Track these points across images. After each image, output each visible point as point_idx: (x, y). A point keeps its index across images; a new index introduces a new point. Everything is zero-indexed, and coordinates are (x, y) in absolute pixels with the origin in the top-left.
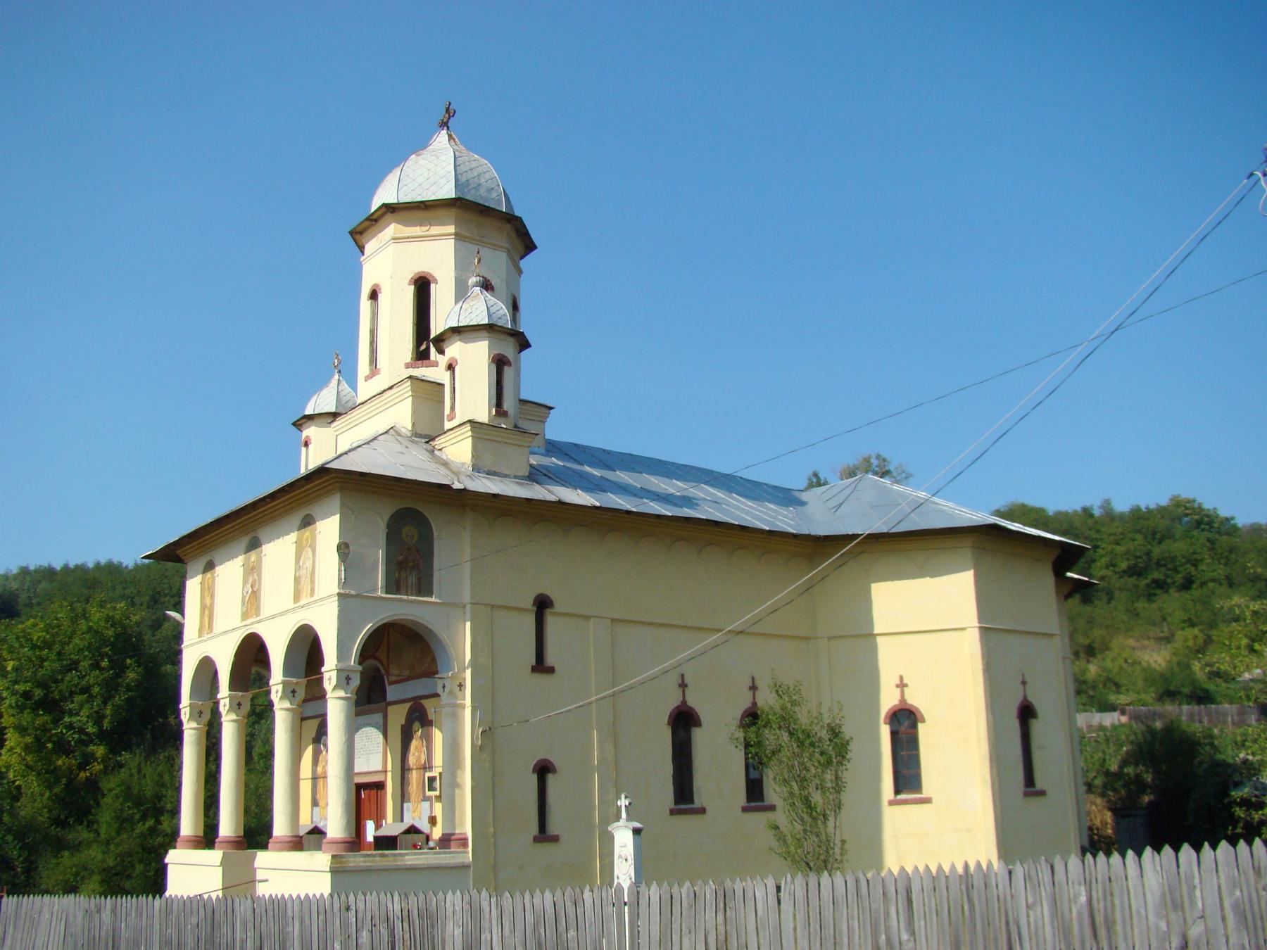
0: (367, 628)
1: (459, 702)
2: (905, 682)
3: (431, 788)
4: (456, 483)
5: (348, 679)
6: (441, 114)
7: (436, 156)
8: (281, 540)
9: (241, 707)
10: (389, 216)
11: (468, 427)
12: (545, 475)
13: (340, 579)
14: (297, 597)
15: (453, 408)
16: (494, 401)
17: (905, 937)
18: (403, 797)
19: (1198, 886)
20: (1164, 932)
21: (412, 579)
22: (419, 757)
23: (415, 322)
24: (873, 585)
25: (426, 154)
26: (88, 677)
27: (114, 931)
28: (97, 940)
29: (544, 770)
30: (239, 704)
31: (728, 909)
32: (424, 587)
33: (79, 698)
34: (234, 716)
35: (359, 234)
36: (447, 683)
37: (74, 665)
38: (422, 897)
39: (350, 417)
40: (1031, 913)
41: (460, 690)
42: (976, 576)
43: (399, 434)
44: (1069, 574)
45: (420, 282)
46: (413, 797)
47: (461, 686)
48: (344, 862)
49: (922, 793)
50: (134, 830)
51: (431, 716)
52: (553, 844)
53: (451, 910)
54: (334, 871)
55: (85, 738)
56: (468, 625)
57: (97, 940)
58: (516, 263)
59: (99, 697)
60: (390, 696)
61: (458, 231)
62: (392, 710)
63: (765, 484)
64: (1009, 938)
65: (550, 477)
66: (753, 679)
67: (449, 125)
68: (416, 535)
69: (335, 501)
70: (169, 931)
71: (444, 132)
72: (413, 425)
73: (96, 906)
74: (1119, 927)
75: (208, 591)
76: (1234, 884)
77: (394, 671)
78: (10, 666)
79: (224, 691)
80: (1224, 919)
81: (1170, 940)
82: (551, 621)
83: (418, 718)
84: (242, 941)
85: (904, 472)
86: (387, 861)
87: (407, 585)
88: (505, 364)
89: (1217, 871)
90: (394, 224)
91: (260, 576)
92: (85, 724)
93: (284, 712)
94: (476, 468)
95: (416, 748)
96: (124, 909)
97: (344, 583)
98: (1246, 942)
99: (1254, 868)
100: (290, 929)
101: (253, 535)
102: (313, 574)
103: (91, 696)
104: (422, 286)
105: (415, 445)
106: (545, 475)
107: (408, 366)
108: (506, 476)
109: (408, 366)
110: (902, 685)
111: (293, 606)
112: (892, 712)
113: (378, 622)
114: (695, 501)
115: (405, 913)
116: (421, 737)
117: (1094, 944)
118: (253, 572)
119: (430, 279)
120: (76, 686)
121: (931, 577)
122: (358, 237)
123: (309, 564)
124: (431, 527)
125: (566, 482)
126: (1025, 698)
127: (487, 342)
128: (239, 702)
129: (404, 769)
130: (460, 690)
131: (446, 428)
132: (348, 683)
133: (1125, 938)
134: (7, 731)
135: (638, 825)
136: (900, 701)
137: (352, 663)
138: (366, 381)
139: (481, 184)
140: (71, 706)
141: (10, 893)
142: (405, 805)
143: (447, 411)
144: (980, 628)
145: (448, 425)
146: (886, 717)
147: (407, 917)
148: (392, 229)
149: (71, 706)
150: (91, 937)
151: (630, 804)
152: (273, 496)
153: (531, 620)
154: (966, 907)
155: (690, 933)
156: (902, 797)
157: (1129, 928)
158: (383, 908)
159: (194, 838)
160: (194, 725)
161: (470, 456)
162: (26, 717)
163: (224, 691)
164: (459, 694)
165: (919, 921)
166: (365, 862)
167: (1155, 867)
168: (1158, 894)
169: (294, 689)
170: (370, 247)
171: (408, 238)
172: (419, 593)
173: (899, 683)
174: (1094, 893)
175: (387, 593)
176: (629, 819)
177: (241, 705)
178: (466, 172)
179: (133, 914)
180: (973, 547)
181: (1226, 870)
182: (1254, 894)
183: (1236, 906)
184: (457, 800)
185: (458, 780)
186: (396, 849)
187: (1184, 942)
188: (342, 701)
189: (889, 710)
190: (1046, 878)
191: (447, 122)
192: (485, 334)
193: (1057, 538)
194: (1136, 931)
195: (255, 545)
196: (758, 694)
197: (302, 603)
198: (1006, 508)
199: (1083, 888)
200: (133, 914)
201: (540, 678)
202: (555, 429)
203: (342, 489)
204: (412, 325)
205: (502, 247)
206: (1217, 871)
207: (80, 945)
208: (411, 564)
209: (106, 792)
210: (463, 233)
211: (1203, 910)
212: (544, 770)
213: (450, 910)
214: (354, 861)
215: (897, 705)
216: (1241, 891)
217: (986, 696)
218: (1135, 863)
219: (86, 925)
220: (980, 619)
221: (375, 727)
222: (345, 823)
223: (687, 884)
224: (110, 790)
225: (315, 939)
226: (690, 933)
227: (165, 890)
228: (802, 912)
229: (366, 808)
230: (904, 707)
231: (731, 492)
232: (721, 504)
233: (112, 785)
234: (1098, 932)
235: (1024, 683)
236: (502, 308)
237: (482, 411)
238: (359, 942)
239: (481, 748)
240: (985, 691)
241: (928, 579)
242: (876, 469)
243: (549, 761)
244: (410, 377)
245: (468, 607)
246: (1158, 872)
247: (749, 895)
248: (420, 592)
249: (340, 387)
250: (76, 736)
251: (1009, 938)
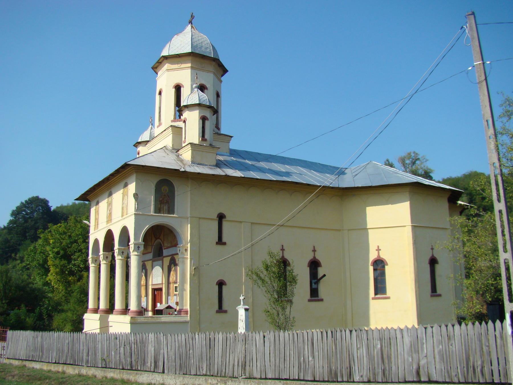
0: (147, 227)
1: (185, 256)
2: (380, 248)
3: (176, 291)
4: (182, 168)
5: (139, 247)
6: (189, 18)
7: (184, 35)
8: (118, 192)
10: (165, 61)
11: (189, 146)
12: (225, 164)
13: (135, 208)
14: (122, 216)
15: (185, 138)
16: (201, 135)
17: (310, 359)
18: (168, 294)
19: (425, 343)
20: (411, 362)
21: (166, 208)
22: (173, 278)
23: (176, 103)
24: (367, 208)
25: (181, 35)
26: (81, 246)
27: (42, 345)
28: (37, 348)
29: (221, 284)
30: (107, 257)
31: (246, 344)
32: (171, 211)
33: (77, 254)
34: (105, 262)
35: (155, 68)
36: (181, 249)
37: (76, 241)
38: (141, 335)
39: (152, 142)
40: (358, 351)
41: (186, 252)
42: (411, 204)
43: (167, 149)
44: (459, 202)
45: (177, 87)
46: (171, 294)
47: (186, 250)
49: (386, 295)
50: (84, 305)
51: (177, 262)
52: (225, 313)
53: (150, 340)
54: (131, 323)
55: (80, 269)
56: (189, 225)
57: (37, 348)
58: (219, 79)
59: (85, 253)
60: (164, 254)
61: (192, 66)
62: (165, 259)
63: (330, 166)
64: (350, 362)
65: (226, 165)
66: (314, 247)
67: (192, 22)
68: (168, 190)
69: (134, 177)
70: (59, 345)
71: (190, 25)
72: (173, 145)
73: (36, 335)
74: (393, 359)
75: (97, 212)
76: (440, 342)
77: (166, 244)
78: (51, 241)
79: (101, 252)
80: (434, 358)
81: (412, 365)
82: (225, 224)
83: (173, 263)
84: (82, 350)
85: (425, 159)
87: (163, 210)
88: (206, 120)
89: (433, 337)
90: (167, 64)
91: (112, 207)
92: (80, 264)
93: (119, 260)
94: (193, 162)
95: (172, 274)
96: (45, 337)
97: (137, 210)
98: (443, 368)
99: (448, 336)
100: (98, 346)
101: (109, 191)
102: (127, 206)
103: (82, 253)
104: (178, 88)
105: (173, 154)
106: (225, 164)
107: (172, 121)
108: (206, 165)
109: (172, 121)
110: (378, 250)
111: (121, 218)
112: (374, 261)
113: (151, 225)
114: (291, 174)
115: (135, 341)
116: (174, 271)
117: (382, 365)
118: (110, 204)
119: (181, 86)
120: (76, 249)
121: (392, 204)
122: (155, 69)
123: (126, 202)
124: (174, 186)
125: (233, 167)
126: (433, 255)
127: (198, 111)
129: (168, 283)
130: (186, 252)
131: (183, 146)
132: (138, 249)
133: (395, 364)
134: (50, 267)
135: (247, 307)
136: (377, 256)
137: (140, 241)
138: (157, 128)
139: (202, 46)
140: (75, 257)
141: (10, 329)
142: (169, 297)
143: (183, 139)
144: (412, 226)
145: (184, 145)
146: (372, 263)
147: (136, 343)
148: (167, 66)
149: (75, 257)
150: (35, 347)
151: (244, 298)
152: (112, 175)
153: (216, 224)
154: (334, 348)
155: (233, 353)
156: (376, 296)
157: (396, 360)
158: (128, 339)
159: (93, 309)
160: (93, 265)
161: (191, 157)
162: (57, 262)
163: (101, 252)
164: (186, 253)
165: (316, 352)
166: (144, 320)
167: (408, 334)
168: (409, 345)
170: (159, 73)
171: (172, 69)
172: (169, 213)
173: (377, 249)
174: (383, 344)
175: (155, 213)
176: (244, 304)
178: (196, 41)
179: (48, 339)
180: (409, 192)
181: (436, 336)
182: (447, 347)
183: (439, 352)
184: (184, 295)
185: (185, 288)
186: (162, 315)
187: (418, 367)
188: (136, 256)
189: (373, 260)
190: (365, 337)
191: (191, 21)
192: (197, 107)
193: (448, 187)
194: (399, 361)
195: (110, 194)
196: (316, 253)
197: (124, 217)
198: (468, 173)
199: (379, 342)
200: (48, 339)
201: (220, 247)
202: (234, 145)
203: (136, 172)
204: (174, 105)
205: (211, 71)
206: (433, 337)
207: (31, 350)
208: (165, 202)
209: (74, 291)
210: (194, 66)
211: (426, 354)
212: (221, 284)
213: (150, 340)
214: (140, 319)
215: (376, 258)
216: (442, 346)
217: (414, 255)
218: (400, 332)
219: (33, 342)
220: (412, 222)
221: (160, 266)
222: (137, 305)
223: (233, 333)
224: (75, 290)
225: (106, 350)
226: (233, 353)
227: (83, 329)
228: (272, 346)
229: (158, 298)
230: (379, 259)
231: (311, 170)
232: (302, 175)
233: (76, 288)
234: (384, 361)
235: (432, 249)
236: (205, 97)
237: (196, 140)
238: (120, 352)
240: (414, 252)
241: (390, 205)
242: (413, 158)
243: (223, 280)
244: (171, 126)
245: (189, 218)
246: (409, 336)
247: (254, 339)
248: (169, 213)
249: (151, 131)
250: (76, 269)
251: (350, 362)
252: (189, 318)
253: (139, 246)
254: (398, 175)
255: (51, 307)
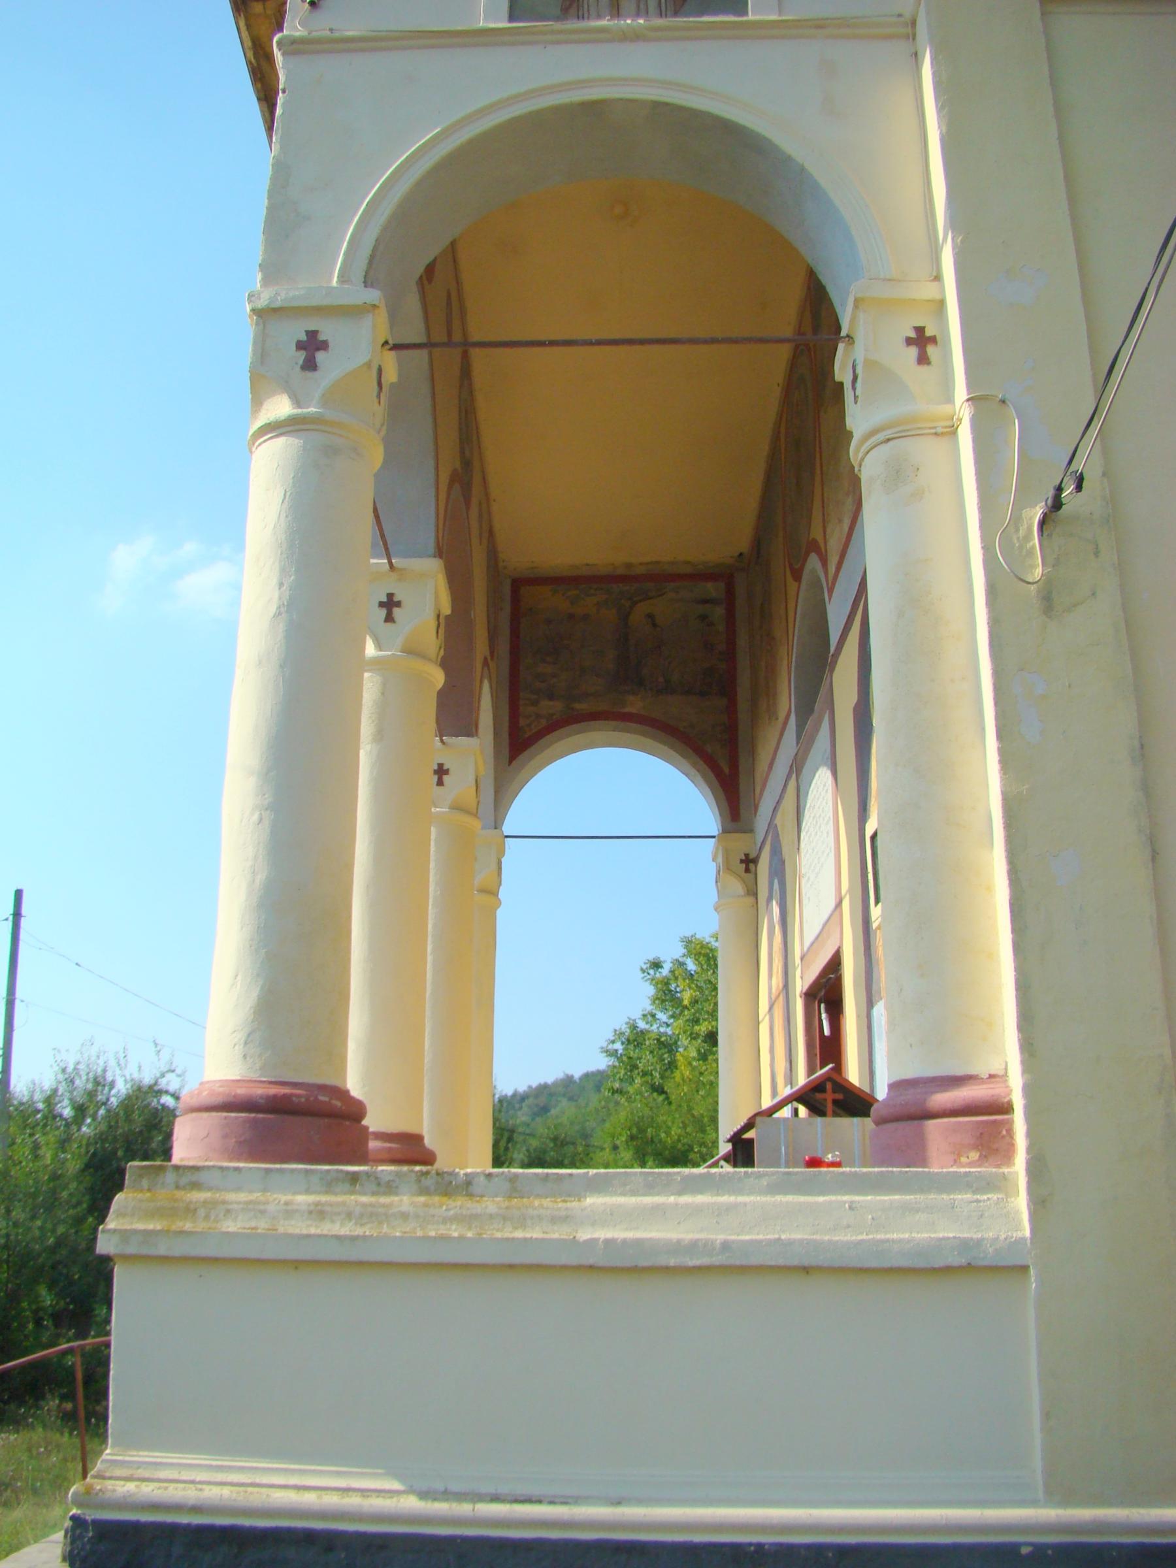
9: (445, 778)
41: (923, 359)
47: (921, 340)
48: (190, 1211)
86: (458, 1219)
128: (440, 766)
130: (923, 359)
132: (310, 365)
166: (319, 1213)
169: (390, 596)
177: (447, 772)
239: (1048, 599)
252: (1021, 1202)
253: (312, 334)
254: (274, 434)
255: (605, 1101)
